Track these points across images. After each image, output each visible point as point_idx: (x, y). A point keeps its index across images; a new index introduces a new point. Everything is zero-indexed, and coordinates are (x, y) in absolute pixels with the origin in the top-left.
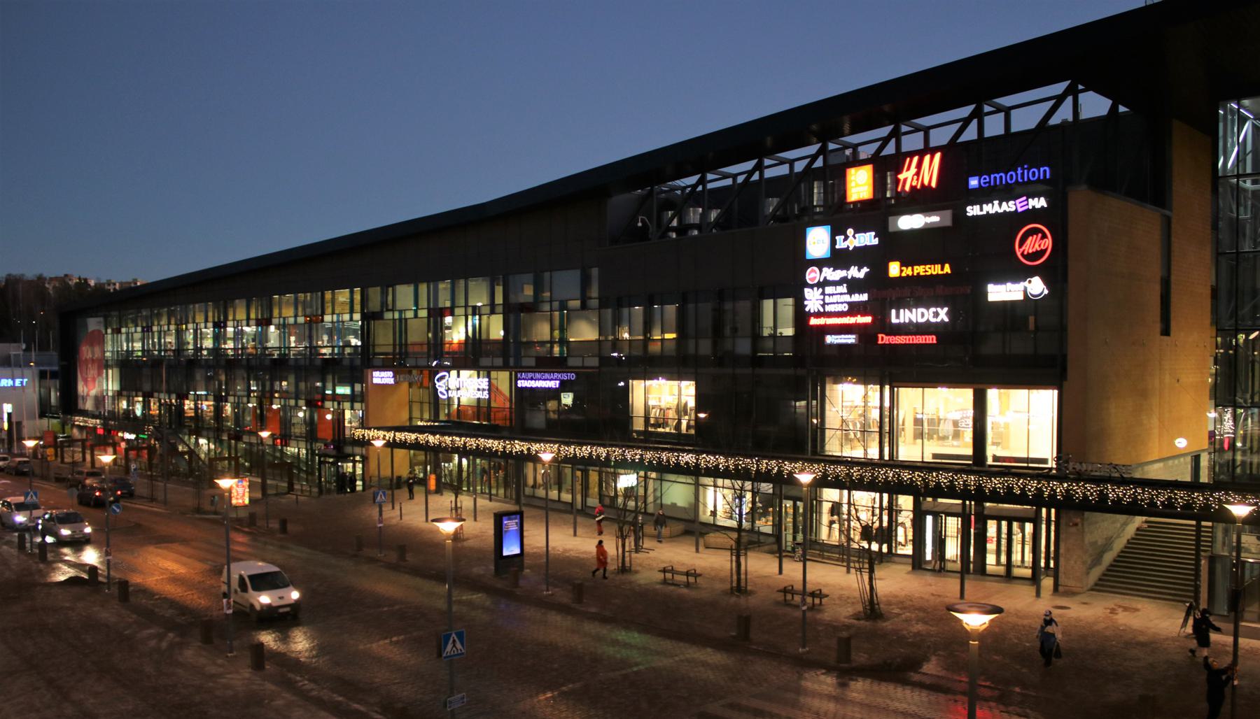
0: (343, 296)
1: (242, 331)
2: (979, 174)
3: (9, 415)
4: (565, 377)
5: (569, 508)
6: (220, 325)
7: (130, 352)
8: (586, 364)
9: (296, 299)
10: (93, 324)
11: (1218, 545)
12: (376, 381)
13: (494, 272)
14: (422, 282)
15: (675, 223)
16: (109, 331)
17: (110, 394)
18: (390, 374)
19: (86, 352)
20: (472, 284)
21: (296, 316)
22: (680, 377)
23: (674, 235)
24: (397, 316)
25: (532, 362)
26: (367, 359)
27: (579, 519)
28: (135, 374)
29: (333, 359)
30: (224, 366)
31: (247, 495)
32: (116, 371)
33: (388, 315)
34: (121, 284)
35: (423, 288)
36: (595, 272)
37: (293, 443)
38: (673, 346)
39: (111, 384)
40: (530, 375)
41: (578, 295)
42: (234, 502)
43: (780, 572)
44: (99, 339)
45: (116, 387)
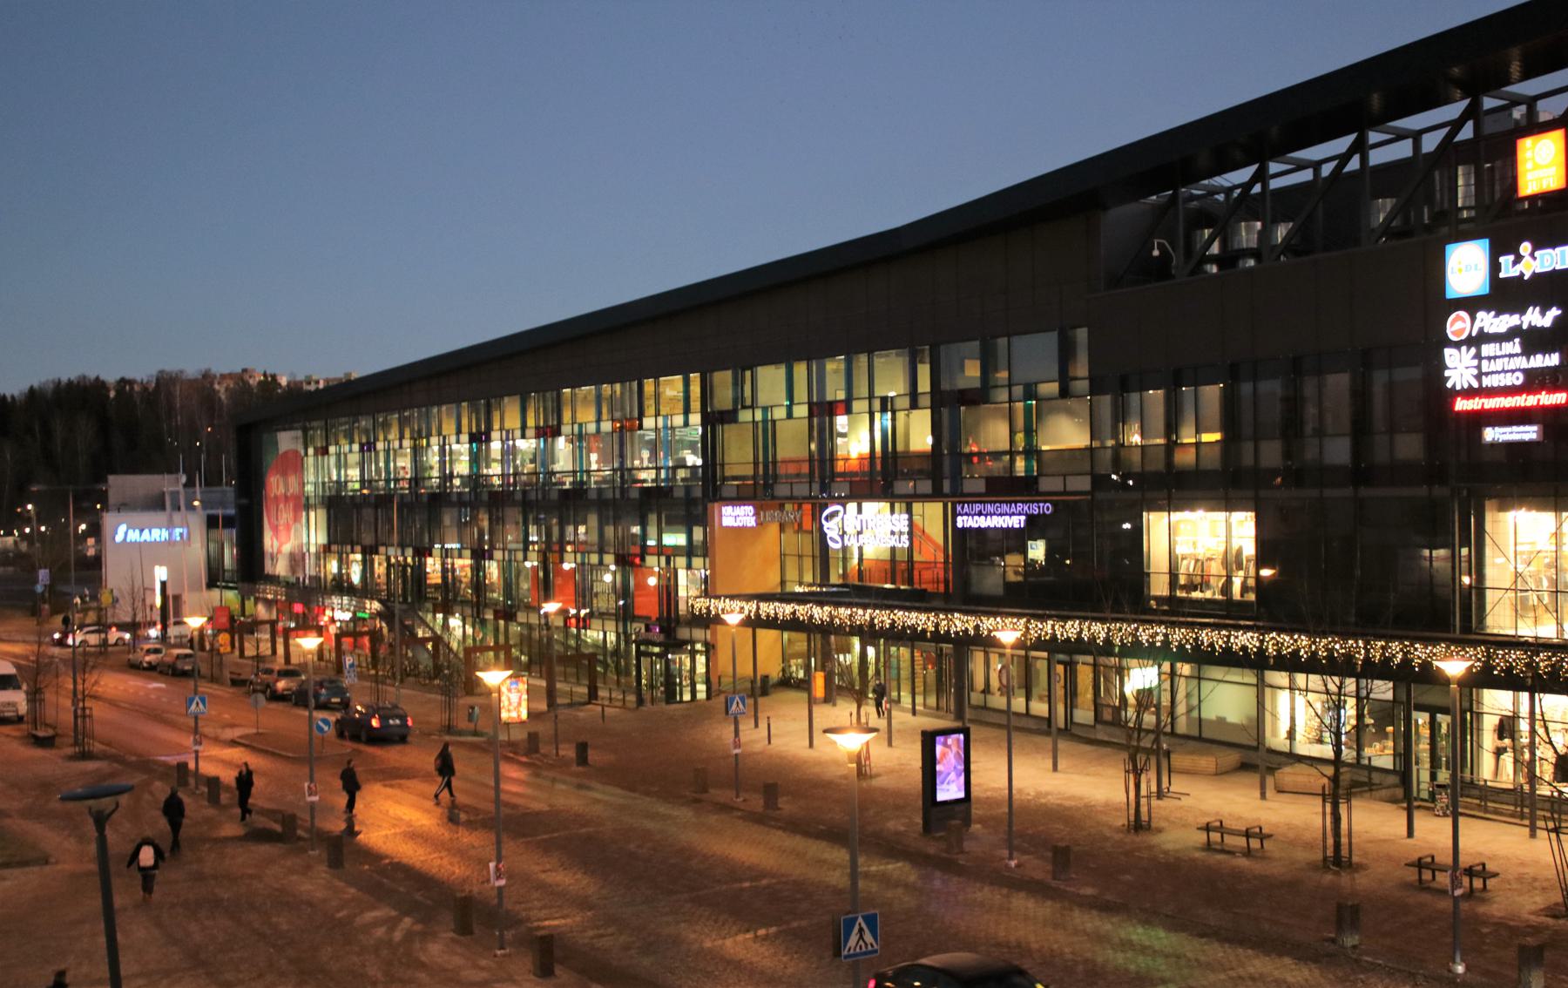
0: (672, 387)
3: (163, 584)
6: (479, 438)
7: (341, 484)
8: (1069, 488)
10: (287, 441)
14: (800, 359)
16: (311, 451)
17: (313, 549)
18: (750, 509)
19: (276, 485)
21: (598, 421)
22: (1229, 505)
26: (712, 486)
30: (487, 502)
31: (524, 704)
33: (745, 416)
39: (314, 532)
40: (977, 507)
42: (504, 715)
44: (294, 464)
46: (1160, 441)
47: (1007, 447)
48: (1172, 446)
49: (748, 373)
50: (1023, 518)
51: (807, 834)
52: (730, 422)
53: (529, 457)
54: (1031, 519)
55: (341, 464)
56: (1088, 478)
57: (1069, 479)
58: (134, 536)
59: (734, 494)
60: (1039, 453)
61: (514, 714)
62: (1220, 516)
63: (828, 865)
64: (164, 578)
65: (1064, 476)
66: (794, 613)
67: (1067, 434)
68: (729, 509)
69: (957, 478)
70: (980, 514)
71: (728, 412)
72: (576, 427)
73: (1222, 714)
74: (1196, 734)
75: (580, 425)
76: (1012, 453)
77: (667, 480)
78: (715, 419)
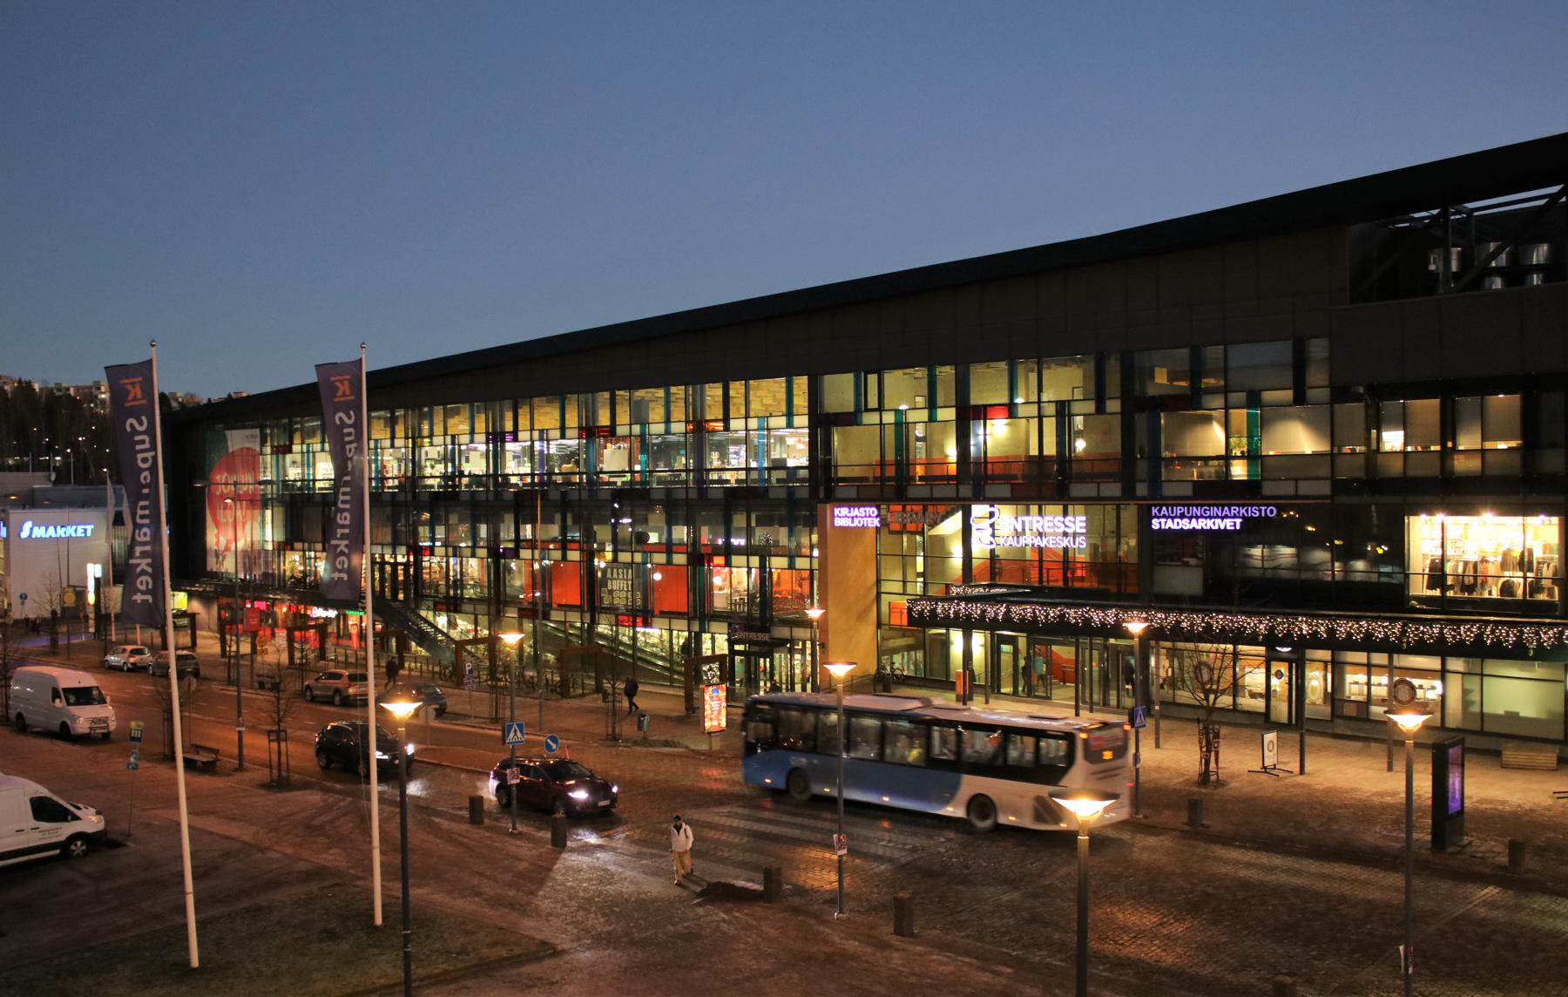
0: (768, 392)
3: (97, 580)
4: (1254, 512)
5: (1261, 721)
6: (497, 438)
7: (307, 482)
8: (1301, 492)
9: (668, 394)
10: (238, 440)
12: (839, 522)
14: (989, 357)
15: (1502, 260)
16: (268, 450)
17: (270, 547)
18: (873, 511)
21: (668, 421)
22: (1525, 509)
23: (1497, 283)
25: (1187, 490)
26: (822, 484)
27: (1163, 724)
28: (304, 514)
29: (446, 493)
30: (488, 502)
31: (724, 712)
32: (280, 511)
33: (872, 418)
34: (77, 388)
36: (1318, 348)
38: (1516, 460)
39: (266, 530)
40: (1178, 510)
42: (708, 724)
43: (1302, 771)
44: (251, 461)
45: (280, 537)
46: (1438, 448)
48: (1447, 454)
49: (873, 379)
50: (1238, 521)
51: (1289, 853)
54: (1246, 521)
55: (308, 461)
56: (1328, 483)
58: (39, 532)
62: (1519, 519)
63: (1383, 886)
64: (99, 575)
65: (1296, 480)
66: (1062, 616)
67: (1299, 439)
68: (844, 511)
70: (1182, 516)
72: (449, 439)
74: (1478, 728)
75: (453, 437)
76: (1227, 458)
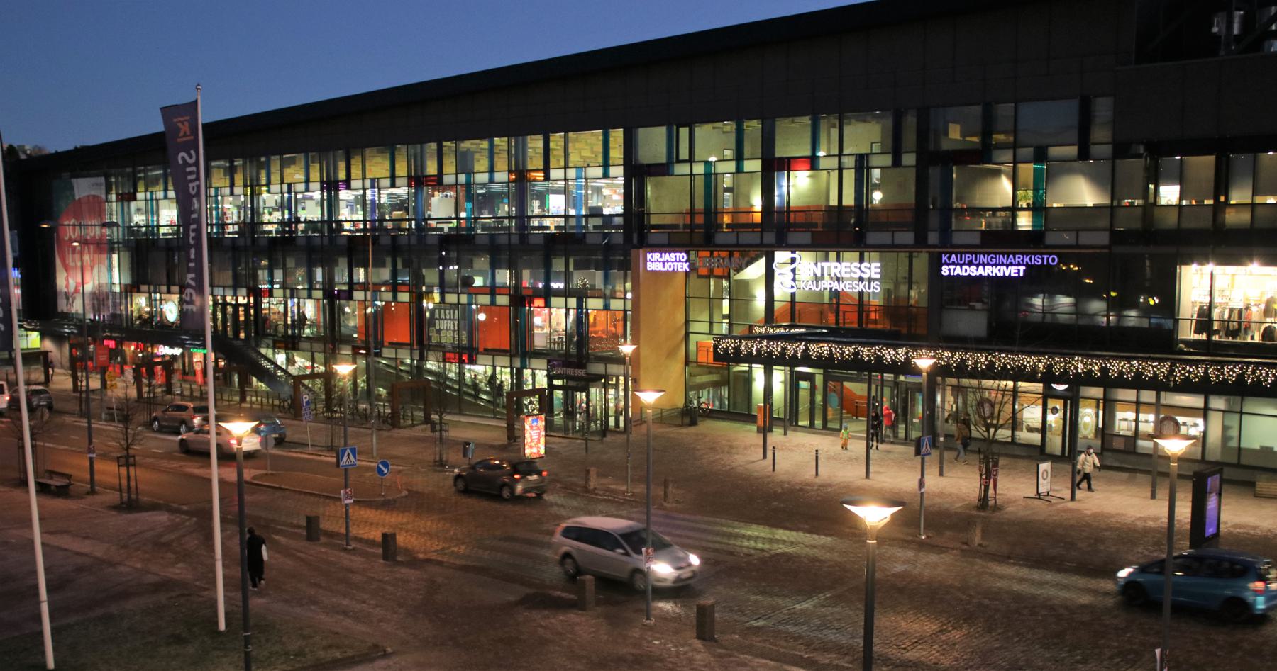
0: (586, 143)
1: (368, 192)
2: (1212, 26)
6: (331, 186)
7: (152, 229)
8: (1081, 242)
9: (492, 146)
10: (84, 187)
11: (819, 380)
12: (650, 267)
13: (388, 145)
16: (114, 197)
17: (117, 289)
19: (70, 230)
20: (702, 131)
24: (699, 169)
26: (636, 231)
28: (151, 259)
30: (322, 247)
31: (543, 440)
32: (126, 256)
33: (682, 169)
35: (753, 127)
37: (481, 358)
39: (113, 274)
40: (967, 258)
41: (388, 174)
42: (528, 451)
45: (127, 280)
47: (1010, 204)
48: (1219, 208)
50: (1022, 268)
52: (664, 175)
53: (163, 203)
54: (1029, 268)
56: (1107, 234)
57: (1081, 233)
59: (666, 242)
60: (1048, 210)
61: (535, 450)
65: (1078, 231)
66: (856, 354)
68: (656, 256)
69: (946, 231)
70: (970, 264)
71: (662, 165)
73: (1268, 444)
74: (1235, 461)
77: (217, 233)
78: (637, 173)
